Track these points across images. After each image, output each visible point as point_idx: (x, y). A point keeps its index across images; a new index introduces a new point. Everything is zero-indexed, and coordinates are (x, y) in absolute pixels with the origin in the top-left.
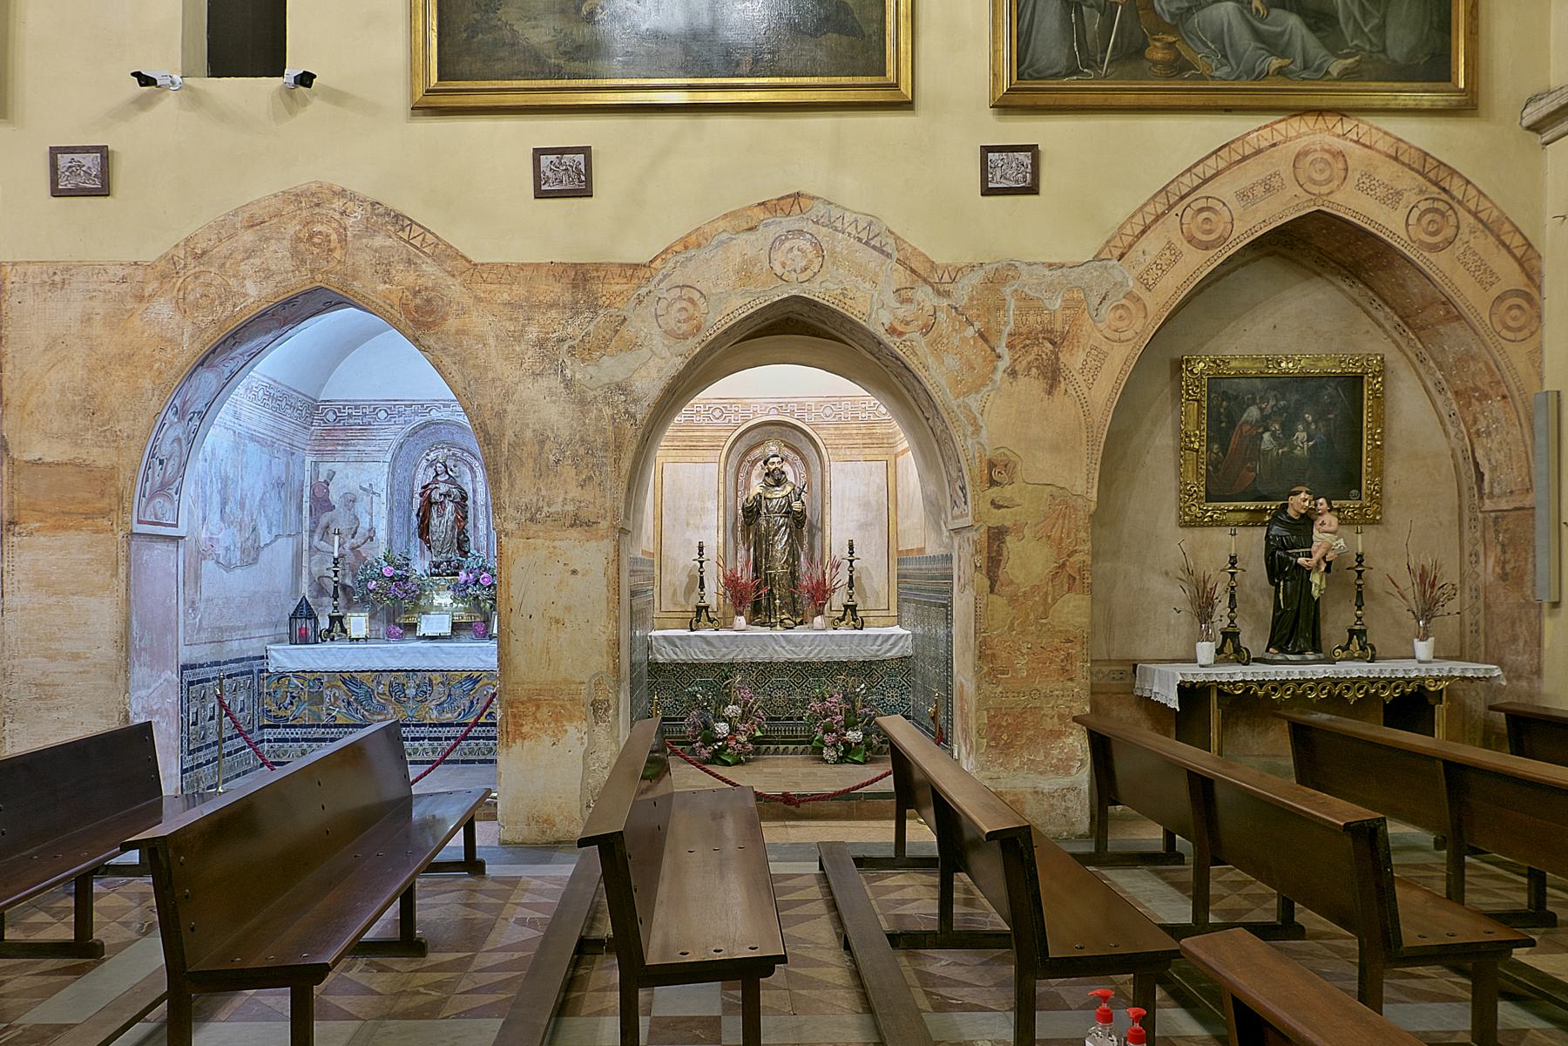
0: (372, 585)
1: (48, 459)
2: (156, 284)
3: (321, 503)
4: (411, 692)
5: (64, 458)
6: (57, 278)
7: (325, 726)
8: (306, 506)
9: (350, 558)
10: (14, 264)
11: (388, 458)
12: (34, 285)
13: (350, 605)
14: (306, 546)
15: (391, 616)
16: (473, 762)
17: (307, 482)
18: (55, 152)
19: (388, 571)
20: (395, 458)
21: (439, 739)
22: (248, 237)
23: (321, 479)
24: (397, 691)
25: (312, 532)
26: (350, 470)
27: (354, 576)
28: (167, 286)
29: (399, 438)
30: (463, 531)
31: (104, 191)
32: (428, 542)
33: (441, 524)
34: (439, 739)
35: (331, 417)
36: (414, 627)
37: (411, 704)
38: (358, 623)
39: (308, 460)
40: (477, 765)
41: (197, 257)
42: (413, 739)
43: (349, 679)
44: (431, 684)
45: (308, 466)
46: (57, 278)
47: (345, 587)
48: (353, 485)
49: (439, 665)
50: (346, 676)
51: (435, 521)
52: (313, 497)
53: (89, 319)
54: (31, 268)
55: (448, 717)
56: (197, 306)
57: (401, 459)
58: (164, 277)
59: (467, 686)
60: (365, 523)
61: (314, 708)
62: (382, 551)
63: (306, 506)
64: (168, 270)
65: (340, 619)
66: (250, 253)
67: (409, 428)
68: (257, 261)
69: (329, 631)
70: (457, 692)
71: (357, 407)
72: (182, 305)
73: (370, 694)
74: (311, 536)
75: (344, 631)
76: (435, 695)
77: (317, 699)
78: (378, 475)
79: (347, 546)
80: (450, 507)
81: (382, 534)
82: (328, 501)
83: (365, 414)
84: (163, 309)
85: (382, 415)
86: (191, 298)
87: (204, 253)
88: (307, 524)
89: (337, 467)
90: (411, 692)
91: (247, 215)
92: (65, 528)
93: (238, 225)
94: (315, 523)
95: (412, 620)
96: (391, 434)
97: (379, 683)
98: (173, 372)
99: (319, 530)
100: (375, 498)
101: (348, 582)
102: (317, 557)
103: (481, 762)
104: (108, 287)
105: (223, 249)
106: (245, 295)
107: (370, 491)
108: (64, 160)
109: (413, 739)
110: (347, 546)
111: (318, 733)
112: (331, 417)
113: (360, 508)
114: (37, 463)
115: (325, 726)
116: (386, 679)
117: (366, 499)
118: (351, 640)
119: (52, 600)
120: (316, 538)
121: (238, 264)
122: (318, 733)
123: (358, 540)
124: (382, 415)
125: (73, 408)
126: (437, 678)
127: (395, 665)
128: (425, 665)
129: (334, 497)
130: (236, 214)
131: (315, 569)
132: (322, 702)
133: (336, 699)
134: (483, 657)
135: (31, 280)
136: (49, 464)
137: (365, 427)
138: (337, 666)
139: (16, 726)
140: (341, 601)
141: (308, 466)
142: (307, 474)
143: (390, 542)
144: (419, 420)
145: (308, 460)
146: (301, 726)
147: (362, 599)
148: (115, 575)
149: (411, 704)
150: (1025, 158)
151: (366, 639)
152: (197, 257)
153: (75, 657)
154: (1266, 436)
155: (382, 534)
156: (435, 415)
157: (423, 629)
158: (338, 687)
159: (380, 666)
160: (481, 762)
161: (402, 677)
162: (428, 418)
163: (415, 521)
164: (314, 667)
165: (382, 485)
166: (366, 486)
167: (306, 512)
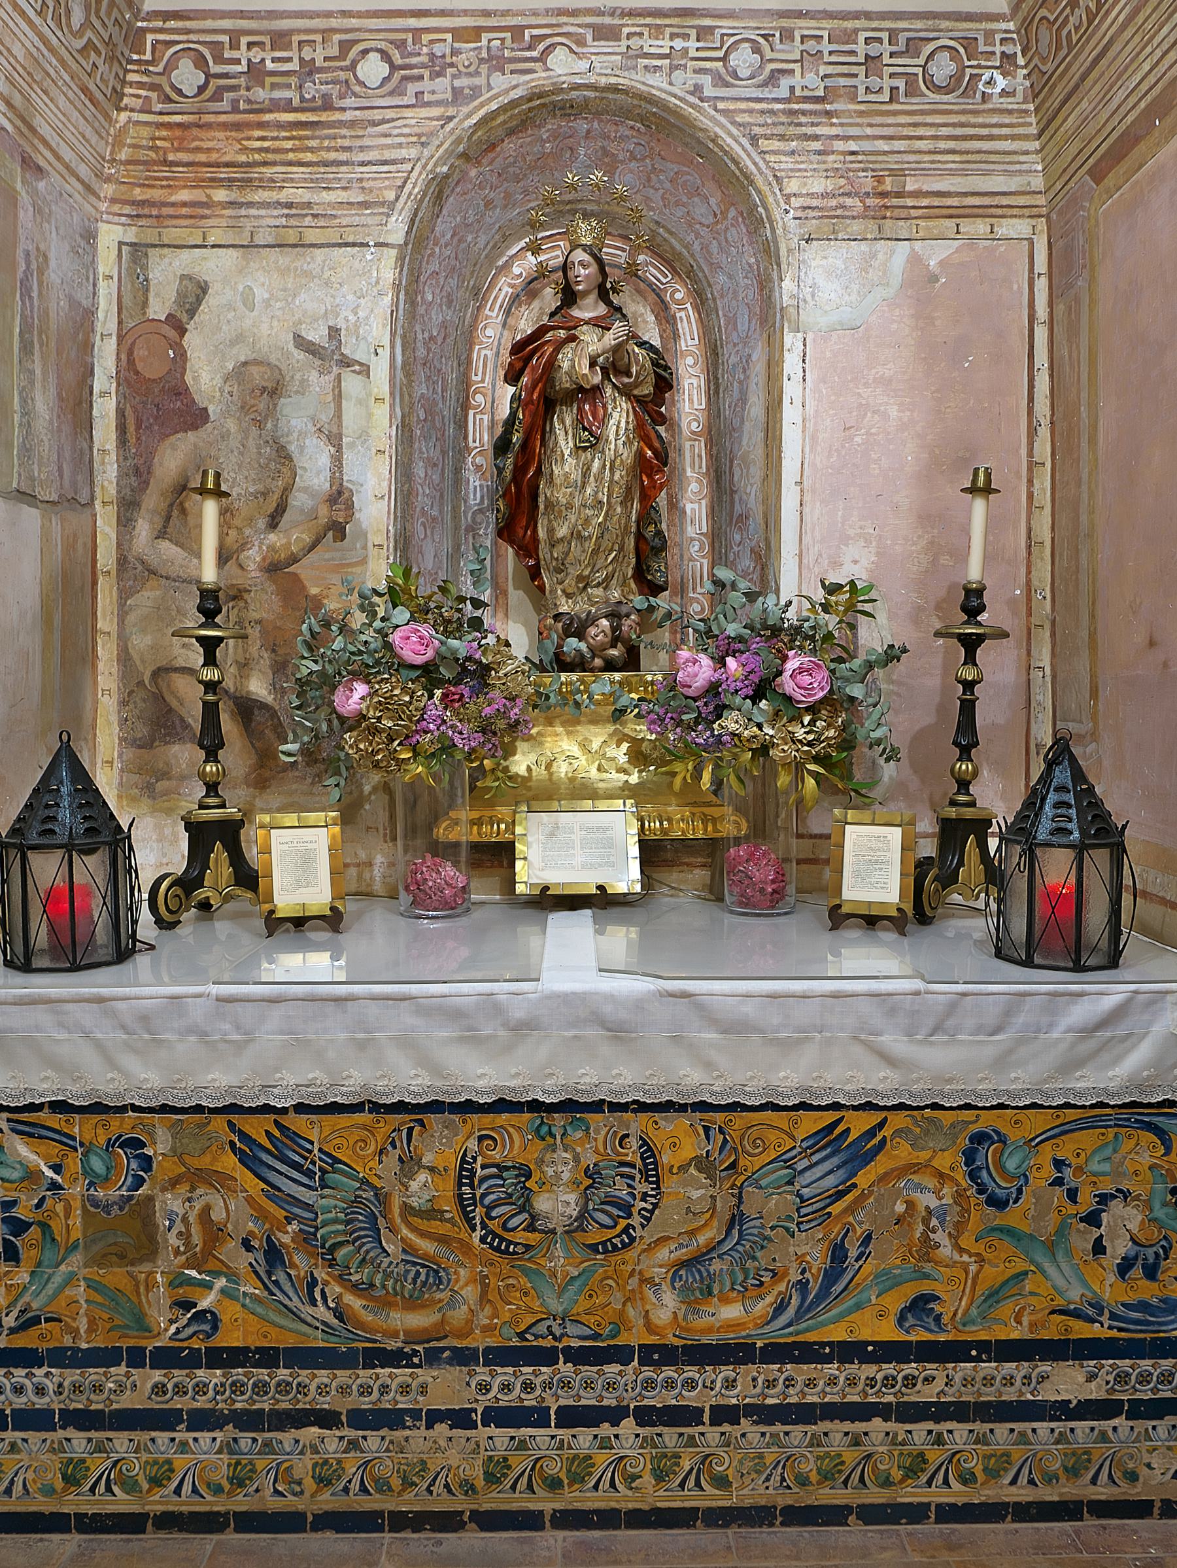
0: (355, 697)
3: (161, 404)
4: (558, 1203)
7: (166, 1358)
8: (105, 409)
9: (264, 604)
11: (397, 229)
13: (266, 771)
14: (106, 557)
15: (416, 820)
16: (915, 1513)
17: (106, 319)
19: (414, 642)
20: (418, 242)
23: (158, 309)
24: (492, 1206)
25: (128, 507)
26: (262, 279)
27: (280, 667)
29: (433, 159)
30: (648, 515)
32: (528, 550)
33: (583, 475)
35: (187, 77)
36: (500, 855)
37: (560, 1259)
38: (299, 855)
39: (110, 235)
40: (854, 1533)
42: (571, 1417)
43: (266, 1136)
44: (651, 1168)
45: (107, 261)
47: (246, 708)
48: (270, 332)
49: (689, 1077)
50: (257, 1128)
51: (565, 459)
52: (129, 375)
55: (729, 1315)
57: (439, 276)
59: (820, 1177)
60: (314, 468)
61: (115, 1276)
62: (378, 571)
63: (105, 409)
65: (229, 833)
67: (469, 117)
69: (188, 883)
70: (770, 1204)
71: (280, 40)
73: (370, 1213)
74: (125, 522)
75: (248, 878)
76: (669, 1217)
77: (127, 1234)
78: (360, 295)
79: (253, 556)
80: (619, 417)
81: (374, 512)
82: (181, 391)
83: (309, 69)
85: (373, 69)
88: (108, 474)
89: (214, 265)
90: (558, 1203)
94: (138, 474)
95: (490, 834)
96: (406, 142)
97: (409, 1164)
99: (152, 500)
100: (352, 383)
101: (258, 687)
102: (146, 598)
103: (872, 1515)
107: (331, 355)
109: (571, 1417)
110: (253, 556)
111: (139, 1388)
112: (187, 77)
113: (297, 418)
115: (166, 1358)
116: (442, 1146)
117: (318, 382)
118: (273, 924)
120: (143, 529)
122: (139, 1388)
123: (291, 536)
124: (373, 69)
126: (680, 1141)
127: (483, 1075)
128: (622, 1077)
129: (205, 377)
131: (140, 642)
132: (147, 1245)
133: (215, 1233)
134: (894, 1041)
137: (315, 119)
138: (218, 1080)
140: (236, 756)
141: (107, 261)
142: (106, 293)
143: (404, 543)
144: (506, 87)
145: (110, 235)
146: (60, 1358)
147: (309, 754)
149: (560, 1259)
151: (333, 920)
154: (361, 689)
155: (374, 512)
156: (563, 67)
157: (530, 872)
158: (221, 1181)
159: (409, 1080)
160: (872, 1515)
161: (515, 1141)
162: (539, 78)
163: (477, 484)
164: (103, 1082)
165: (372, 326)
166: (317, 334)
167: (105, 434)
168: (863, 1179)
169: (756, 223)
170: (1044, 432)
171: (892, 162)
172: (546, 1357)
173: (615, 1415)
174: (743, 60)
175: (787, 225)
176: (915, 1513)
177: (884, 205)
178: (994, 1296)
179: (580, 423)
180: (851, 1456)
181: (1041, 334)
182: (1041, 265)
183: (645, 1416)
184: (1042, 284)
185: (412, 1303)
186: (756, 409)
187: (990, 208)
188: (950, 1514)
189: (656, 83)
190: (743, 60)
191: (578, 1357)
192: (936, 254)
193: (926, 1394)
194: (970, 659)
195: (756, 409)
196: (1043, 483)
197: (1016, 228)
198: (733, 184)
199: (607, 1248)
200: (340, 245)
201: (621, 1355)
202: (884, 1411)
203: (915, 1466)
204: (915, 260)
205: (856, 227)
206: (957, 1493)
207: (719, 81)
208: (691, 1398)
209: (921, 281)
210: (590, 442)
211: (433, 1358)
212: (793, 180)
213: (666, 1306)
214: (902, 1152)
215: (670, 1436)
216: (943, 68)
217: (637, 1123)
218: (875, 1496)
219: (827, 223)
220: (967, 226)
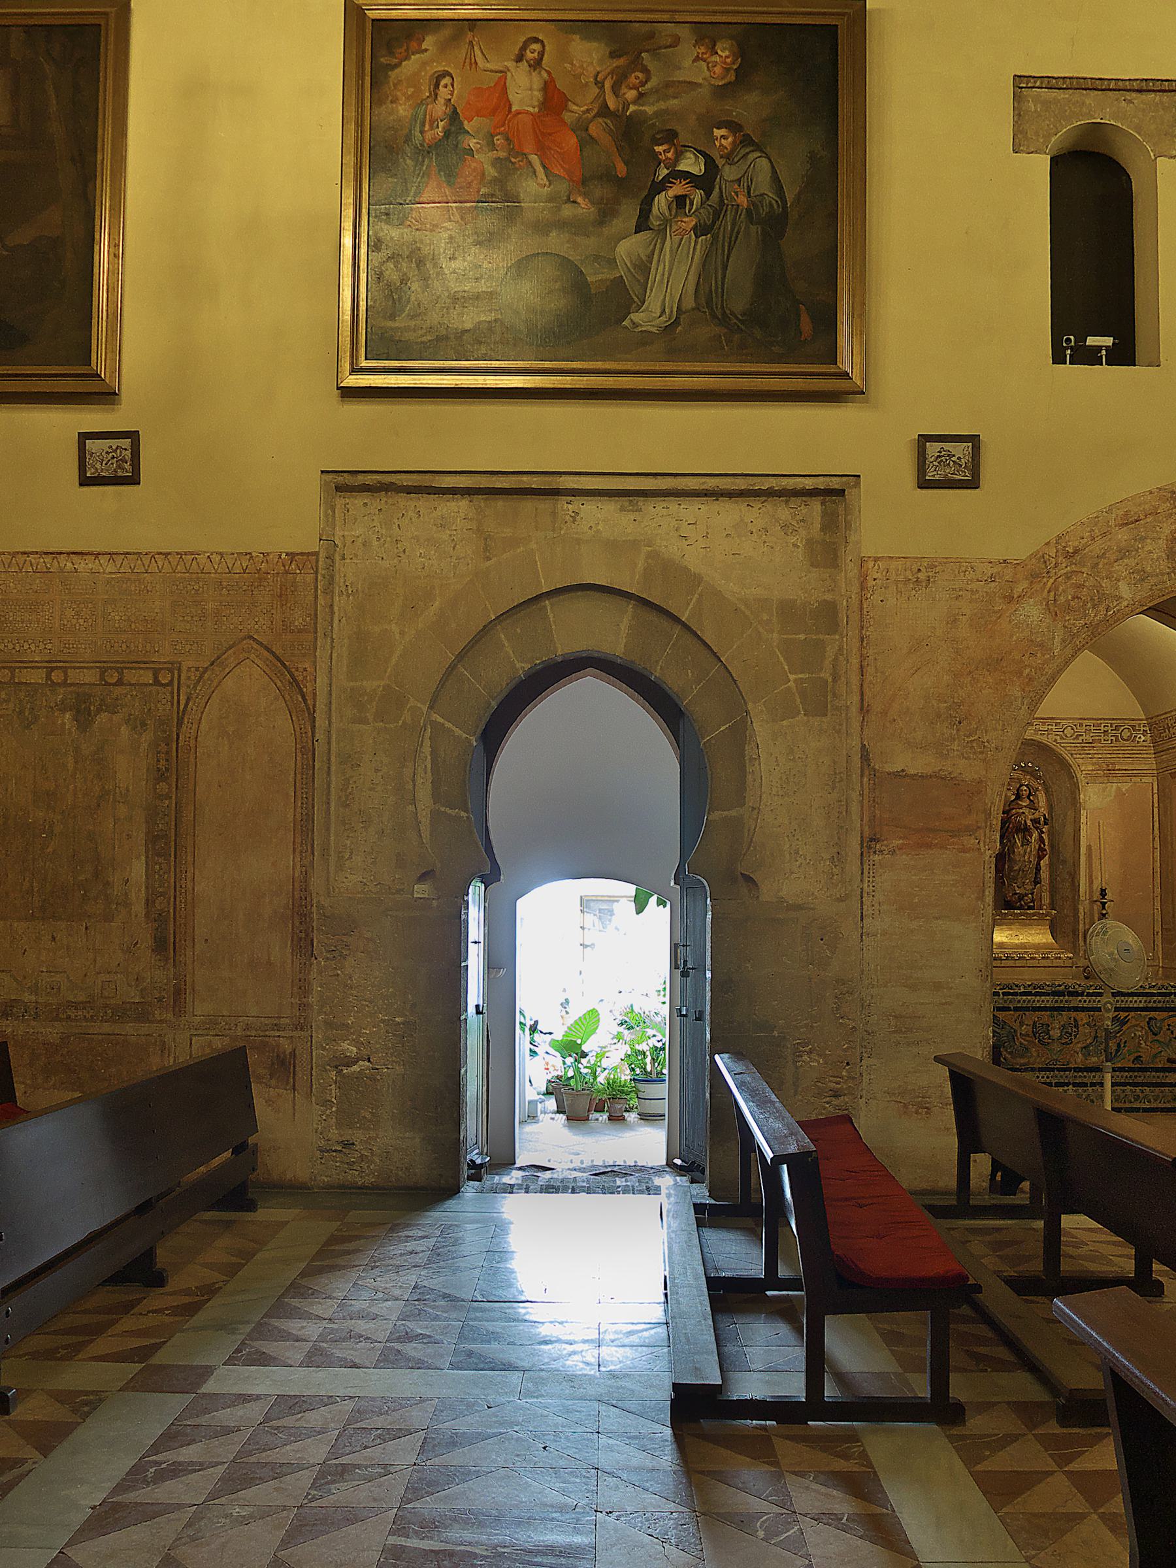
1: (912, 772)
2: (1025, 584)
5: (928, 771)
6: (922, 576)
10: (876, 559)
12: (897, 582)
16: (1138, 1110)
18: (925, 439)
21: (1085, 1085)
22: (1123, 536)
28: (1037, 587)
31: (973, 484)
34: (1085, 1085)
37: (1057, 1047)
41: (1068, 556)
42: (1058, 1085)
44: (1076, 1026)
46: (922, 576)
53: (955, 620)
54: (893, 565)
56: (1068, 609)
58: (1034, 576)
64: (1038, 570)
66: (1124, 553)
68: (1131, 562)
72: (1053, 609)
84: (1032, 611)
86: (1062, 599)
87: (1076, 551)
91: (1121, 513)
92: (929, 846)
93: (1112, 523)
97: (1022, 1024)
98: (1043, 679)
104: (974, 586)
105: (1096, 548)
106: (1119, 598)
108: (933, 449)
114: (901, 775)
119: (914, 925)
121: (1111, 564)
125: (939, 716)
130: (1109, 511)
135: (893, 578)
136: (913, 777)
139: (872, 1061)
148: (981, 898)
149: (1057, 1047)
150: (961, 450)
152: (1068, 556)
153: (937, 986)
168: (1124, 1028)
169: (1071, 776)
170: (1157, 839)
171: (1112, 761)
172: (1053, 1070)
173: (1068, 1084)
174: (1068, 731)
175: (1081, 777)
176: (1138, 1110)
177: (1110, 772)
178: (1155, 1056)
179: (1024, 837)
180: (1122, 1096)
181: (1156, 810)
182: (1155, 791)
183: (1075, 1085)
184: (1156, 796)
185: (1022, 1057)
186: (1069, 829)
187: (1139, 774)
188: (1145, 1110)
189: (1044, 739)
190: (1068, 731)
191: (1059, 1070)
192: (1125, 787)
193: (1140, 1080)
194: (1104, 908)
195: (1069, 829)
196: (1157, 854)
197: (1149, 779)
198: (1065, 766)
199: (1066, 1043)
200: (128, 553)
201: (1069, 1070)
202: (1130, 1084)
203: (1137, 1098)
204: (1118, 789)
205: (1101, 780)
206: (1147, 1105)
207: (1062, 738)
208: (1085, 1080)
209: (1120, 795)
210: (1026, 842)
211: (1026, 1070)
212: (1083, 767)
213: (1080, 1057)
214: (1134, 1022)
215: (1080, 1089)
216: (1126, 734)
217: (1073, 1014)
218: (1128, 1105)
219: (1092, 779)
220: (1134, 779)
